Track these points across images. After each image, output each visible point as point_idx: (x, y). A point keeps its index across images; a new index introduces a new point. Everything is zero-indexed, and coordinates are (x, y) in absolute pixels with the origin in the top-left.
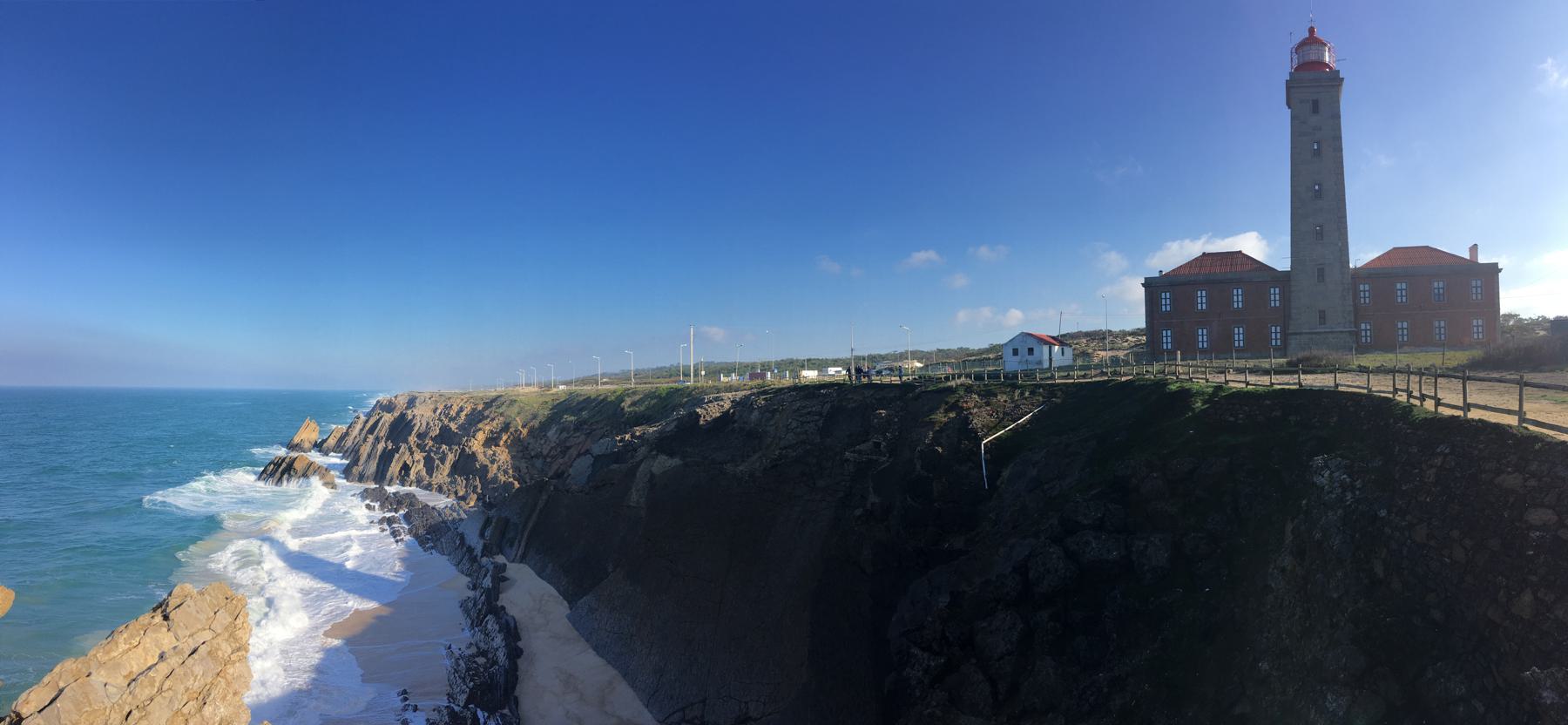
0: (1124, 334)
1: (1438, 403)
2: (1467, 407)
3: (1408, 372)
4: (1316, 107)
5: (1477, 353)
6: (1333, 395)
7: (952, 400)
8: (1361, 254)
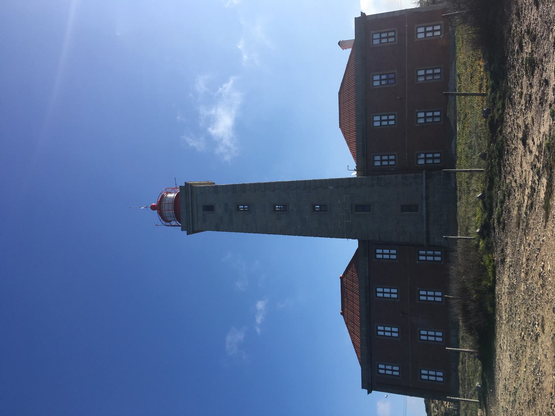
4: (209, 208)
5: (463, 35)
8: (339, 162)
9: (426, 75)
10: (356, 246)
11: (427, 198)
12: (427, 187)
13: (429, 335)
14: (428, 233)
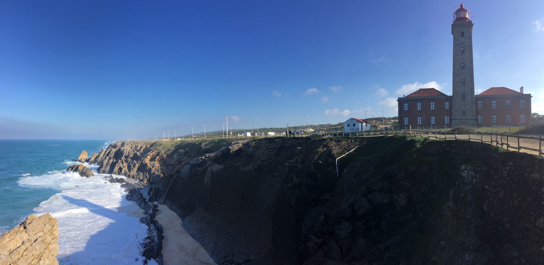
0: (390, 119)
1: (508, 146)
2: (519, 148)
4: (463, 34)
5: (523, 128)
6: (468, 143)
7: (325, 143)
10: (448, 95)
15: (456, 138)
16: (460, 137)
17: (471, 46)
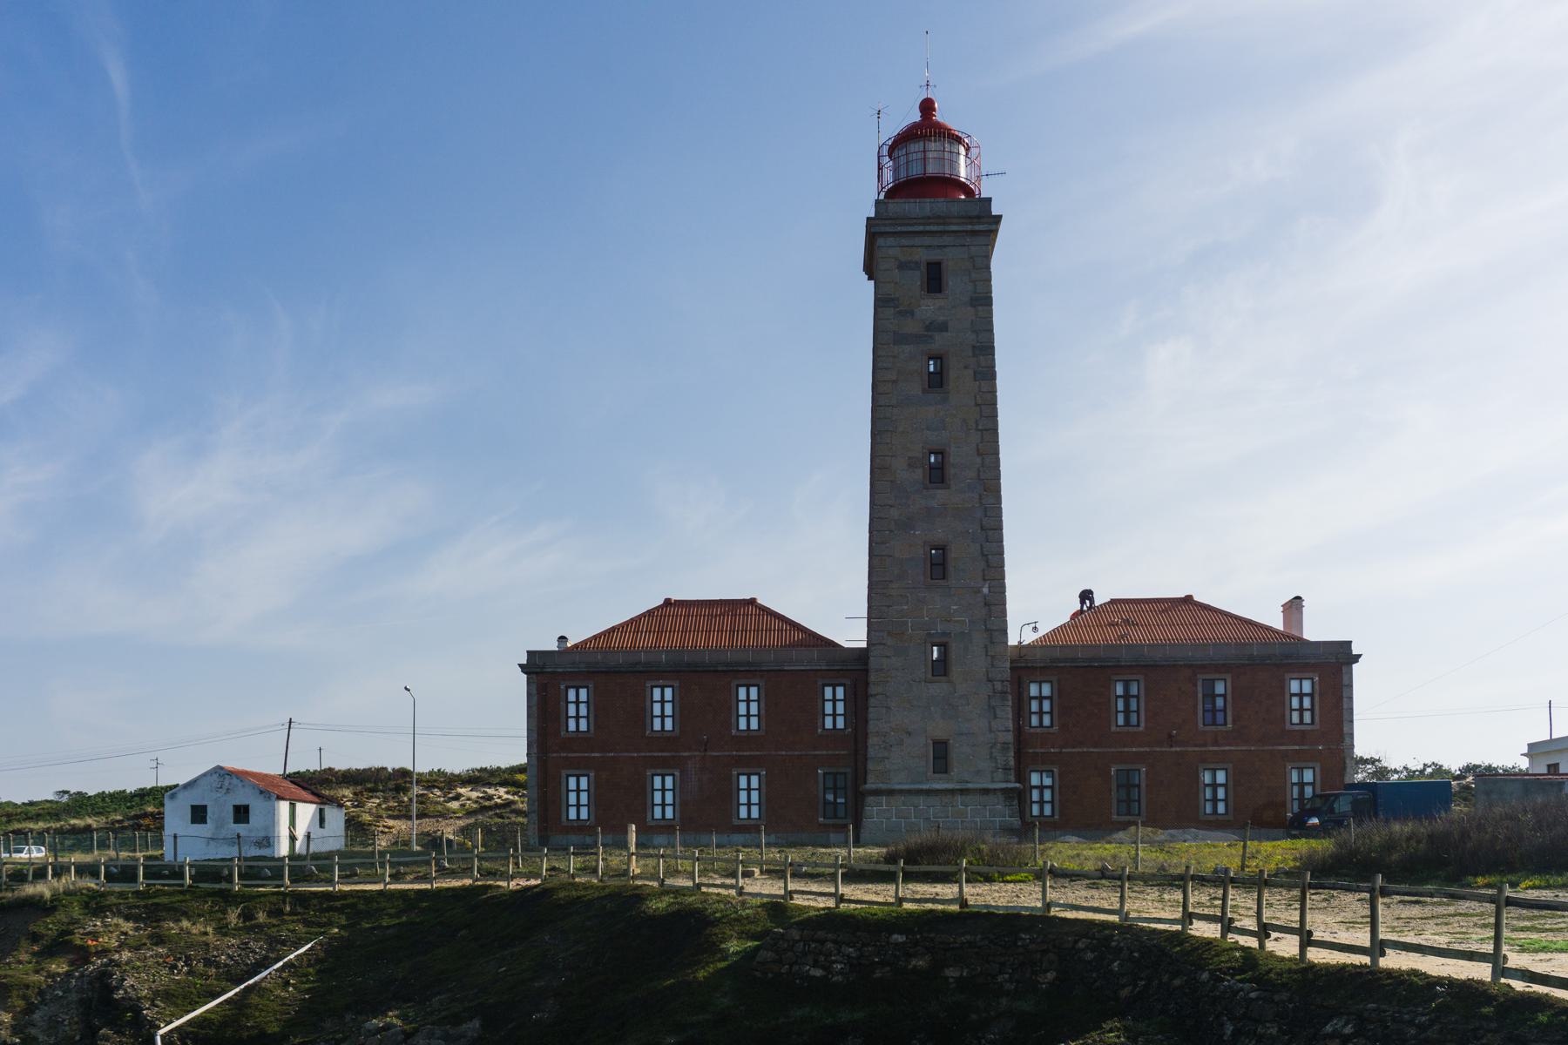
0: (446, 782)
1: (1307, 940)
2: (1378, 947)
3: (1220, 879)
4: (934, 279)
6: (1040, 923)
7: (49, 926)
8: (1035, 606)
9: (1214, 786)
11: (963, 792)
12: (986, 791)
13: (663, 795)
14: (890, 793)
15: (963, 903)
16: (983, 895)
17: (986, 349)
